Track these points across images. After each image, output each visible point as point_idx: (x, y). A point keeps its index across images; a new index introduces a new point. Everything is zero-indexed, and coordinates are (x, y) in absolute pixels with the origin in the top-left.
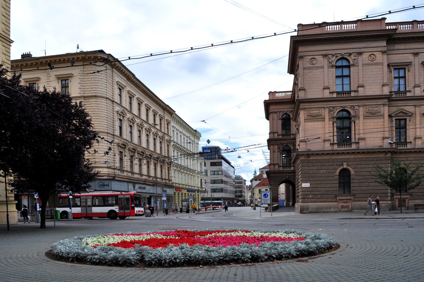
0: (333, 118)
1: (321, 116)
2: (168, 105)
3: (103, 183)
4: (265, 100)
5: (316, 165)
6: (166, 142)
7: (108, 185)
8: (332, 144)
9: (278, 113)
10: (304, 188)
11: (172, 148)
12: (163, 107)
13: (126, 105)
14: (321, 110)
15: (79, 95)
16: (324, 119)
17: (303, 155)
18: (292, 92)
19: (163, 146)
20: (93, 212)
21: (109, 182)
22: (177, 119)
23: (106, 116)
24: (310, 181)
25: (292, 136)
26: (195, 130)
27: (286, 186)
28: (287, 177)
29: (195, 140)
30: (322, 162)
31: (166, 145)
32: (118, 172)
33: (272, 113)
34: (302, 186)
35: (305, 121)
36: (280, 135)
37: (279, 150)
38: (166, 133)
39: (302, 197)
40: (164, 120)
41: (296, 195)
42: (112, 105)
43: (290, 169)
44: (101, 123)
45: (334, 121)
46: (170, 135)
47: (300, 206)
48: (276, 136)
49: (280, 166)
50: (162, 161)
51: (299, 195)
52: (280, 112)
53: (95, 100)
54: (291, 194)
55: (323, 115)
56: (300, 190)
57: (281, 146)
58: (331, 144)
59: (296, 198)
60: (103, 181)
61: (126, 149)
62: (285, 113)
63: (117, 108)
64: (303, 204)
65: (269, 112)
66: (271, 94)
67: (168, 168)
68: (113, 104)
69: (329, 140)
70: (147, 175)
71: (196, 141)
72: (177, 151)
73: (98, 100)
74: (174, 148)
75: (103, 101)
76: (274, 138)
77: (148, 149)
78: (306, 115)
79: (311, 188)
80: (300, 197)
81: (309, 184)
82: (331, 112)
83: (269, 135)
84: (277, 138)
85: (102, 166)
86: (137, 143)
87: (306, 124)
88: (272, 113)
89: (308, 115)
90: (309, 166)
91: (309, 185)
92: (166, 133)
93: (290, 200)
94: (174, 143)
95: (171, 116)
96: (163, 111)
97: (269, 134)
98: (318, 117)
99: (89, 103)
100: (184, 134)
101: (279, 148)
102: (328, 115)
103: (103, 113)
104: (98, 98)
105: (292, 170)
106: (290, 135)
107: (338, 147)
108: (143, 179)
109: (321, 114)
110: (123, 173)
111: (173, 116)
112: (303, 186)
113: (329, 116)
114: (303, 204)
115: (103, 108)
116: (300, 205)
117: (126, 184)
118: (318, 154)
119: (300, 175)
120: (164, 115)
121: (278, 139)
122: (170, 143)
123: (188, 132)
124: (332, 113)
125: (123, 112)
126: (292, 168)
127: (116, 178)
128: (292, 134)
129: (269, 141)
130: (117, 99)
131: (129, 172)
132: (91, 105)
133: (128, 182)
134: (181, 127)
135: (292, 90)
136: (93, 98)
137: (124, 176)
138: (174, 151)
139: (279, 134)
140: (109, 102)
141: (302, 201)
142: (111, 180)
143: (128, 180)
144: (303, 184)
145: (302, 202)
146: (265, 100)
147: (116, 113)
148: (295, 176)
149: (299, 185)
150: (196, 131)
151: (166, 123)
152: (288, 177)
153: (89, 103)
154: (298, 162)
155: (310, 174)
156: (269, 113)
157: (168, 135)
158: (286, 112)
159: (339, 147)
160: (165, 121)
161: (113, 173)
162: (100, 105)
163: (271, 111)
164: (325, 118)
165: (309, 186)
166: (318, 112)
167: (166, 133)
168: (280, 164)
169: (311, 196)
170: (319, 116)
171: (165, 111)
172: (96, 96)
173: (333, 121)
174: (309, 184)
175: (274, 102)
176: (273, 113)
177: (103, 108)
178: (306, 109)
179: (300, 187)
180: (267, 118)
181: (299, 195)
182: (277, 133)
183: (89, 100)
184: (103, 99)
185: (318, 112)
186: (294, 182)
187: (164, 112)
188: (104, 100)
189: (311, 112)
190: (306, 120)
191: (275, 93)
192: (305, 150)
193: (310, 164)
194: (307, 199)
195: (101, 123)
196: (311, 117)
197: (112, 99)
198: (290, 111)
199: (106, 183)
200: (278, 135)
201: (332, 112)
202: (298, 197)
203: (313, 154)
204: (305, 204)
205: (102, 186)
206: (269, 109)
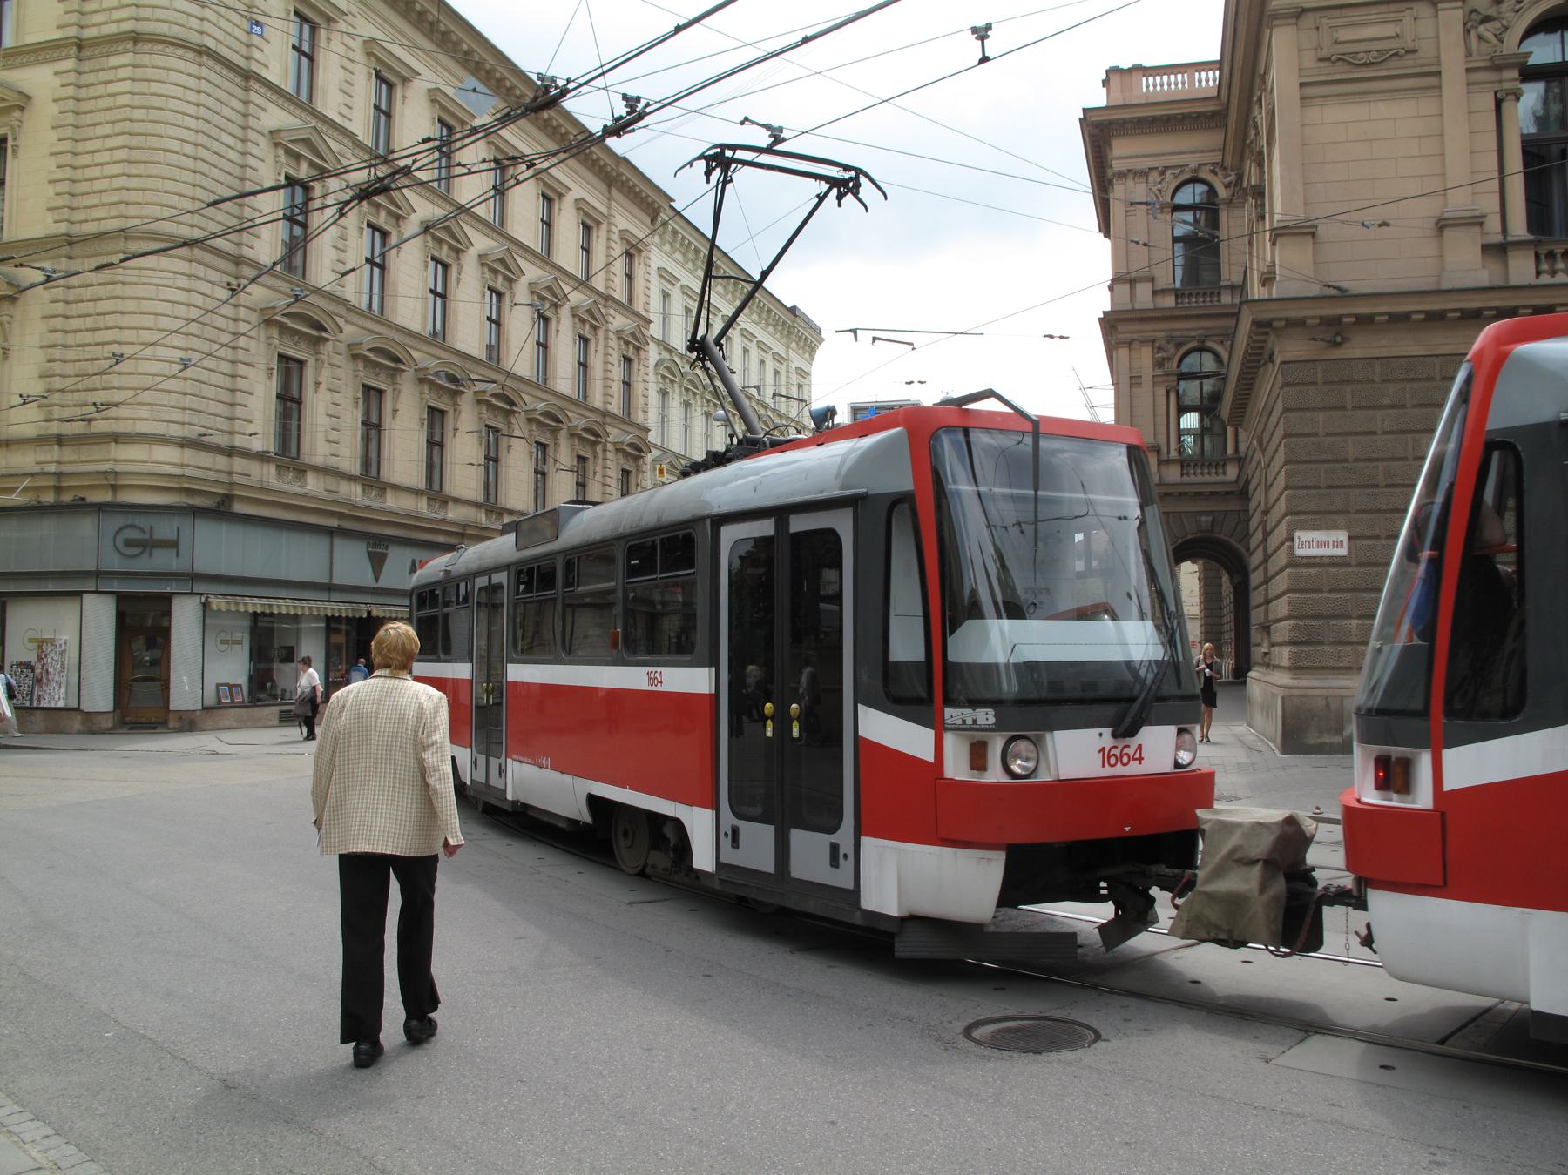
0: (1498, 68)
1: (1409, 60)
2: (625, 159)
3: (142, 530)
4: (1085, 110)
5: (1386, 401)
6: (613, 343)
7: (173, 545)
8: (1498, 250)
9: (1154, 176)
10: (1311, 562)
11: (652, 377)
12: (607, 173)
13: (345, 111)
14: (1408, 20)
15: (58, 35)
16: (1432, 81)
17: (1300, 323)
18: (1219, 64)
19: (596, 362)
20: (923, 660)
21: (184, 523)
22: (683, 238)
23: (188, 149)
24: (1348, 512)
25: (1226, 299)
26: (789, 305)
27: (1205, 578)
28: (1203, 518)
29: (792, 353)
30: (1433, 379)
31: (615, 358)
32: (354, 492)
33: (1122, 175)
34: (1292, 548)
35: (1302, 98)
36: (1163, 291)
37: (1160, 372)
38: (619, 295)
39: (1293, 629)
40: (609, 231)
41: (1256, 616)
42: (240, 93)
43: (1220, 478)
44: (159, 184)
45: (1506, 85)
46: (640, 310)
47: (1283, 698)
48: (1144, 293)
49: (1168, 461)
50: (629, 450)
51: (1271, 617)
52: (1163, 173)
53: (127, 58)
54: (1228, 618)
55: (1426, 50)
56: (1280, 583)
57: (1172, 351)
58: (1485, 248)
59: (1255, 636)
60: (143, 521)
61: (327, 348)
62: (1186, 176)
63: (275, 117)
64: (1304, 683)
65: (1110, 173)
66: (1115, 79)
67: (626, 473)
68: (247, 89)
69: (1478, 221)
70: (481, 499)
71: (796, 361)
72: (681, 395)
73: (145, 59)
74: (664, 377)
75: (180, 65)
76: (1137, 306)
77: (542, 383)
78: (1309, 60)
79: (1360, 565)
80: (1282, 630)
81: (1343, 536)
82: (1481, 29)
83: (1108, 294)
84: (1151, 306)
85: (144, 430)
86: (416, 326)
87: (1314, 113)
88: (1122, 175)
89: (1325, 53)
90: (1344, 408)
91: (1339, 544)
92: (617, 296)
93: (1225, 649)
94: (666, 355)
95: (653, 220)
96: (603, 187)
97: (1111, 288)
98: (1394, 67)
99: (103, 76)
100: (762, 346)
101: (1159, 364)
102: (1461, 52)
103: (172, 131)
104: (148, 47)
105: (1232, 483)
106: (1216, 292)
107: (1538, 273)
108: (445, 521)
109: (1410, 45)
110: (298, 478)
111: (675, 232)
112: (1299, 552)
113: (1469, 54)
114: (1304, 683)
115: (173, 104)
116: (1287, 692)
117: (322, 542)
118: (1399, 320)
119: (1283, 498)
120: (609, 208)
121: (1155, 309)
122: (638, 349)
123: (768, 324)
124: (1489, 36)
125: (315, 139)
126: (1232, 472)
127: (238, 508)
128: (1226, 287)
129: (1110, 323)
130: (277, 62)
131: (351, 478)
132: (112, 88)
133: (330, 532)
134: (730, 296)
135: (1217, 57)
136: (120, 48)
137: (304, 496)
138: (664, 393)
139: (1161, 284)
140: (211, 71)
141: (1295, 657)
142: (196, 512)
143: (334, 523)
144: (1302, 536)
145: (1297, 668)
146: (1085, 110)
147: (263, 142)
148: (1244, 517)
149: (1271, 573)
150: (793, 311)
151: (618, 249)
152: (1210, 518)
153: (103, 76)
154: (1269, 382)
155: (1346, 460)
156: (1111, 182)
157: (627, 307)
158: (1196, 170)
159: (1545, 266)
160: (615, 237)
161: (224, 478)
162: (155, 87)
163: (1117, 166)
164: (1438, 73)
165: (1343, 552)
166: (1389, 30)
167: (619, 295)
168: (1164, 449)
169: (1354, 622)
170: (1395, 62)
171: (614, 192)
172: (136, 38)
173: (1496, 87)
174: (1343, 536)
175: (1131, 121)
176: (1130, 176)
177: (173, 104)
178: (1311, 16)
179: (1281, 558)
180: (1105, 227)
181: (1271, 617)
182: (1152, 280)
183: (103, 62)
184: (180, 52)
185: (1389, 30)
186: (1239, 547)
187: (610, 193)
188: (183, 63)
189: (1345, 35)
190: (1309, 91)
191: (1136, 75)
192: (1315, 290)
193: (1348, 389)
194: (1329, 649)
195: (159, 184)
196: (1347, 68)
197: (242, 63)
198: (1213, 164)
199: (164, 529)
200: (1155, 293)
201: (1489, 25)
202: (1266, 629)
203: (1365, 321)
204: (1315, 683)
205: (136, 551)
206: (1109, 157)
